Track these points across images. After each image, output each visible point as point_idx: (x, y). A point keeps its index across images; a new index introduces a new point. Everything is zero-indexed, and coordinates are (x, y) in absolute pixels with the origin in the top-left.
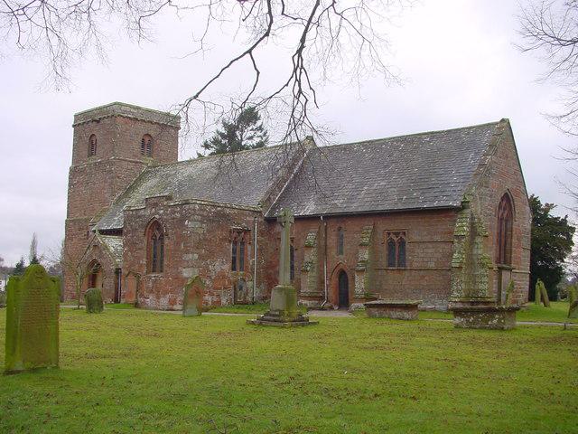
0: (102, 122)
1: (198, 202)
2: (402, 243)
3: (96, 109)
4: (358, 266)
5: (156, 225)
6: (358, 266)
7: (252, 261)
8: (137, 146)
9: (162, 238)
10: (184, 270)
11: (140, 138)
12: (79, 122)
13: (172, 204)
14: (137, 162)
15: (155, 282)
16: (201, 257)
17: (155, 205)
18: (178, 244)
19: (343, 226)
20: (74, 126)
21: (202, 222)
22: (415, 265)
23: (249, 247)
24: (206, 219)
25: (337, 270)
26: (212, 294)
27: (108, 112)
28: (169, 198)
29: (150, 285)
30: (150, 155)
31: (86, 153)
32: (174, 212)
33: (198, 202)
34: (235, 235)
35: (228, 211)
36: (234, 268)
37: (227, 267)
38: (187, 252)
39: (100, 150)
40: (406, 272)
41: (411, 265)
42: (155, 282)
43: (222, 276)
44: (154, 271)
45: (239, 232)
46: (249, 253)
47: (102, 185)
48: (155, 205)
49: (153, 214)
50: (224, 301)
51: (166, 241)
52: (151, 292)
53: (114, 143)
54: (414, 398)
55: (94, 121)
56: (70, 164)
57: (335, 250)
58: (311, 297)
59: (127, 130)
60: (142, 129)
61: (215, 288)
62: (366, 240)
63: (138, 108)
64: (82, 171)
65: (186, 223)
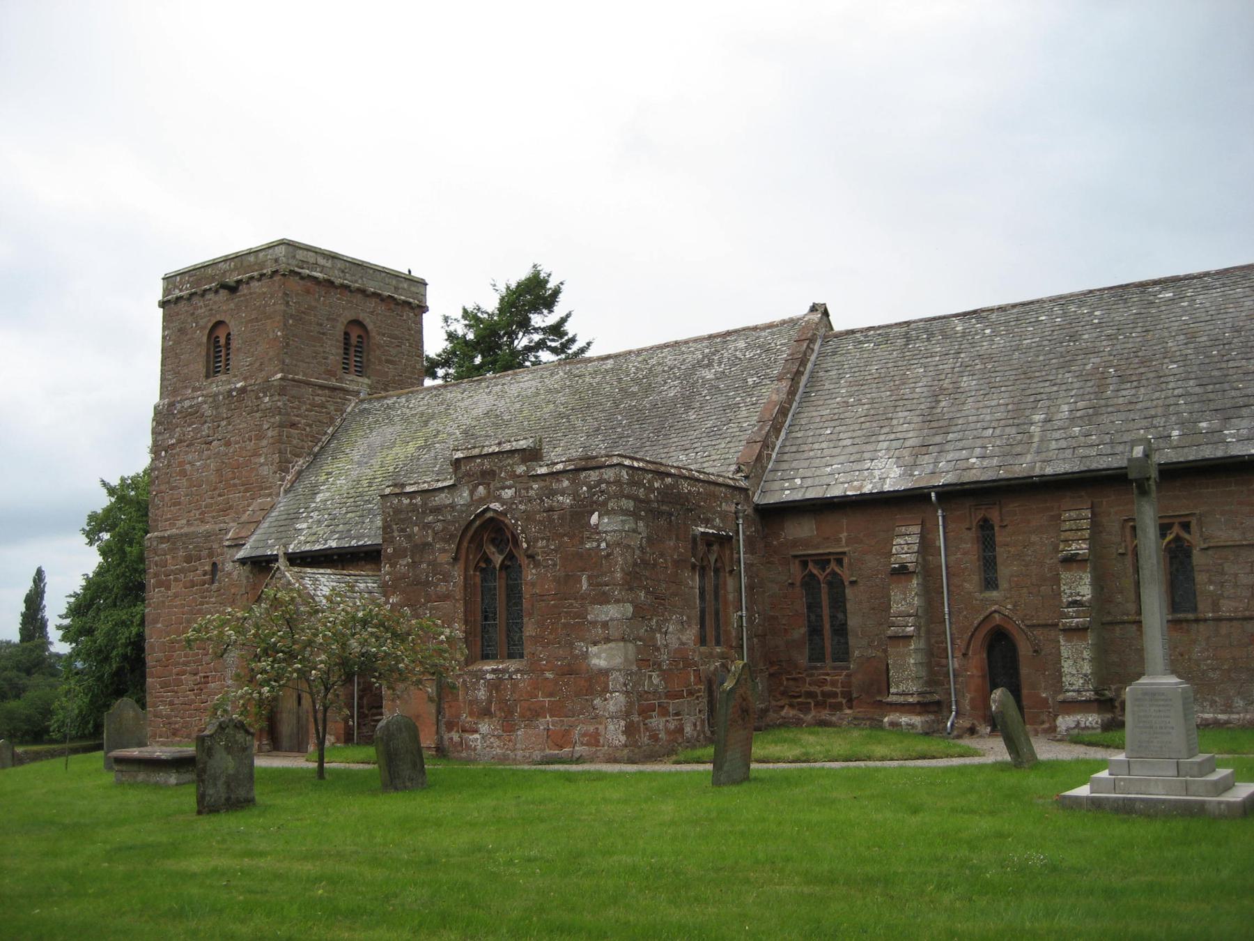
0: (244, 289)
1: (627, 462)
2: (836, 585)
3: (226, 259)
4: (1067, 616)
5: (489, 532)
6: (1067, 616)
7: (738, 617)
8: (334, 352)
9: (511, 566)
10: (593, 649)
11: (340, 328)
12: (177, 293)
13: (544, 470)
14: (334, 389)
15: (495, 686)
16: (640, 613)
17: (487, 476)
18: (570, 579)
19: (994, 516)
20: (163, 304)
21: (635, 515)
22: (1227, 608)
23: (730, 583)
24: (644, 509)
25: (977, 642)
26: (664, 712)
27: (262, 265)
28: (532, 455)
29: (482, 694)
30: (360, 373)
31: (200, 367)
32: (552, 493)
33: (627, 462)
34: (701, 548)
35: (685, 487)
36: (702, 640)
37: (690, 635)
38: (604, 599)
39: (240, 361)
40: (1202, 627)
41: (1216, 606)
42: (495, 686)
43: (682, 660)
44: (485, 657)
45: (708, 540)
46: (731, 597)
47: (251, 445)
48: (487, 476)
49: (482, 500)
50: (688, 729)
51: (530, 574)
52: (486, 713)
53: (281, 335)
54: (529, 860)
55: (224, 286)
56: (156, 398)
57: (976, 578)
58: (922, 707)
59: (311, 308)
60: (346, 310)
61: (671, 695)
62: (1081, 548)
63: (333, 257)
64: (193, 414)
65: (594, 519)
